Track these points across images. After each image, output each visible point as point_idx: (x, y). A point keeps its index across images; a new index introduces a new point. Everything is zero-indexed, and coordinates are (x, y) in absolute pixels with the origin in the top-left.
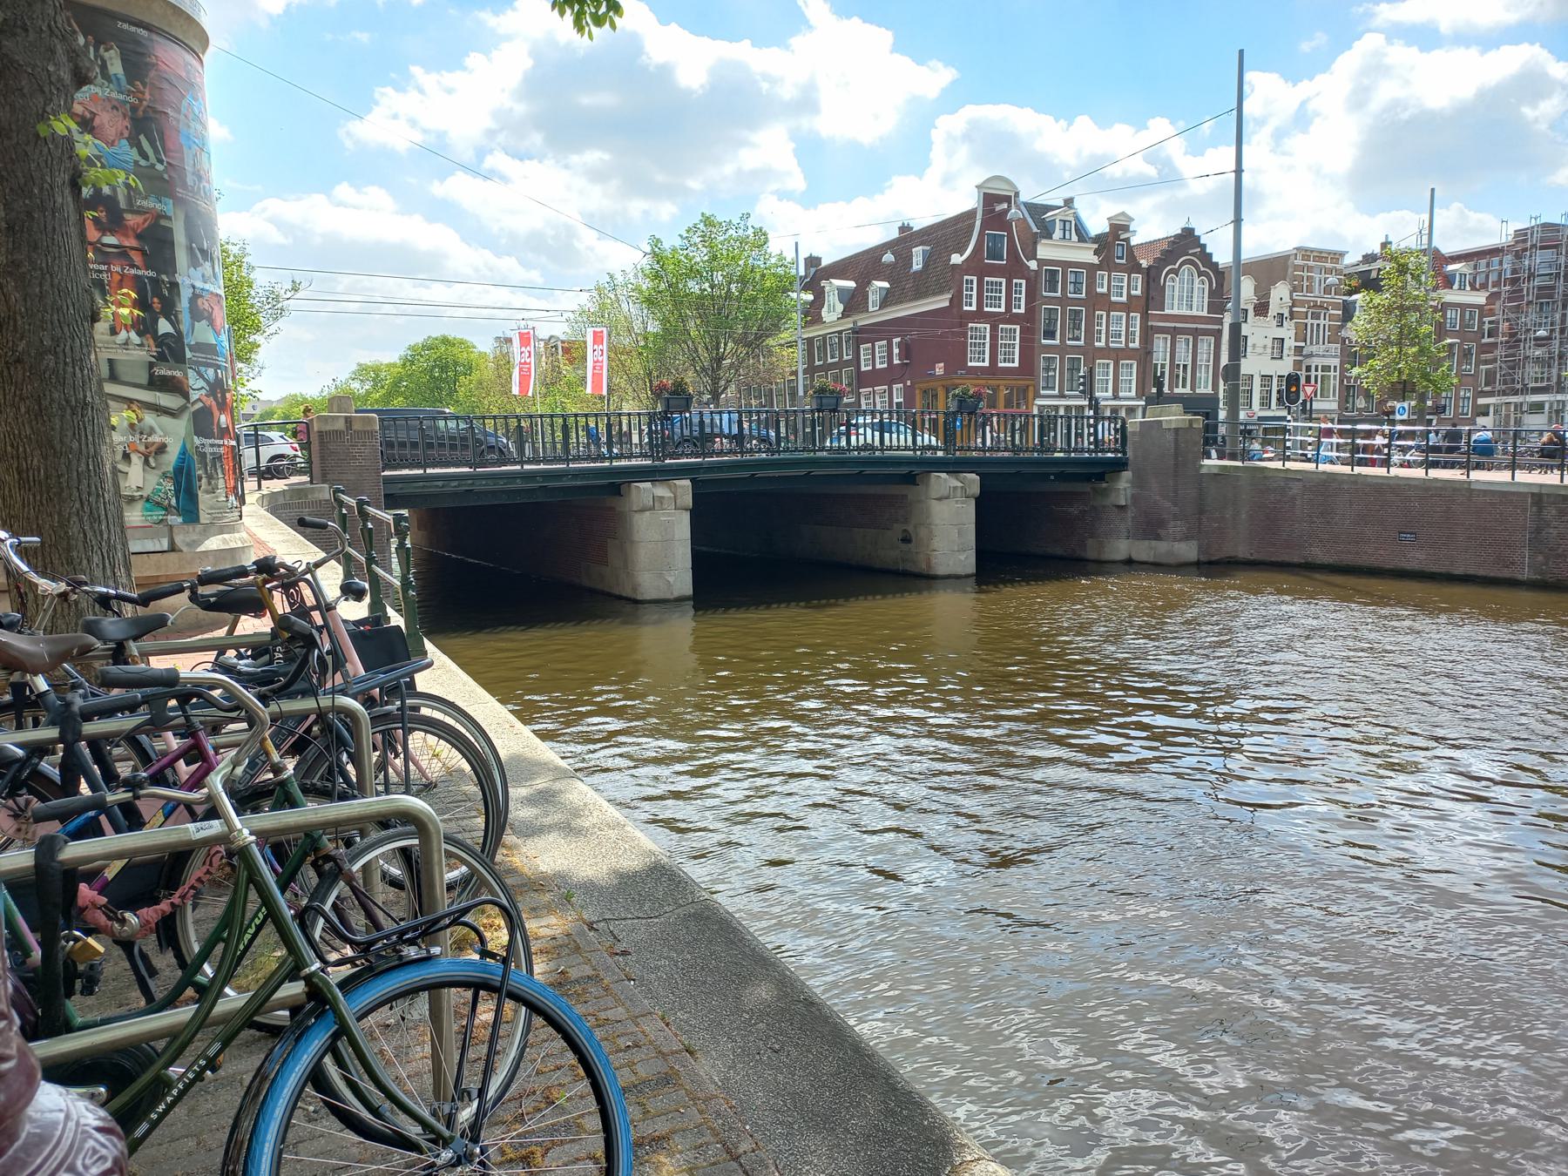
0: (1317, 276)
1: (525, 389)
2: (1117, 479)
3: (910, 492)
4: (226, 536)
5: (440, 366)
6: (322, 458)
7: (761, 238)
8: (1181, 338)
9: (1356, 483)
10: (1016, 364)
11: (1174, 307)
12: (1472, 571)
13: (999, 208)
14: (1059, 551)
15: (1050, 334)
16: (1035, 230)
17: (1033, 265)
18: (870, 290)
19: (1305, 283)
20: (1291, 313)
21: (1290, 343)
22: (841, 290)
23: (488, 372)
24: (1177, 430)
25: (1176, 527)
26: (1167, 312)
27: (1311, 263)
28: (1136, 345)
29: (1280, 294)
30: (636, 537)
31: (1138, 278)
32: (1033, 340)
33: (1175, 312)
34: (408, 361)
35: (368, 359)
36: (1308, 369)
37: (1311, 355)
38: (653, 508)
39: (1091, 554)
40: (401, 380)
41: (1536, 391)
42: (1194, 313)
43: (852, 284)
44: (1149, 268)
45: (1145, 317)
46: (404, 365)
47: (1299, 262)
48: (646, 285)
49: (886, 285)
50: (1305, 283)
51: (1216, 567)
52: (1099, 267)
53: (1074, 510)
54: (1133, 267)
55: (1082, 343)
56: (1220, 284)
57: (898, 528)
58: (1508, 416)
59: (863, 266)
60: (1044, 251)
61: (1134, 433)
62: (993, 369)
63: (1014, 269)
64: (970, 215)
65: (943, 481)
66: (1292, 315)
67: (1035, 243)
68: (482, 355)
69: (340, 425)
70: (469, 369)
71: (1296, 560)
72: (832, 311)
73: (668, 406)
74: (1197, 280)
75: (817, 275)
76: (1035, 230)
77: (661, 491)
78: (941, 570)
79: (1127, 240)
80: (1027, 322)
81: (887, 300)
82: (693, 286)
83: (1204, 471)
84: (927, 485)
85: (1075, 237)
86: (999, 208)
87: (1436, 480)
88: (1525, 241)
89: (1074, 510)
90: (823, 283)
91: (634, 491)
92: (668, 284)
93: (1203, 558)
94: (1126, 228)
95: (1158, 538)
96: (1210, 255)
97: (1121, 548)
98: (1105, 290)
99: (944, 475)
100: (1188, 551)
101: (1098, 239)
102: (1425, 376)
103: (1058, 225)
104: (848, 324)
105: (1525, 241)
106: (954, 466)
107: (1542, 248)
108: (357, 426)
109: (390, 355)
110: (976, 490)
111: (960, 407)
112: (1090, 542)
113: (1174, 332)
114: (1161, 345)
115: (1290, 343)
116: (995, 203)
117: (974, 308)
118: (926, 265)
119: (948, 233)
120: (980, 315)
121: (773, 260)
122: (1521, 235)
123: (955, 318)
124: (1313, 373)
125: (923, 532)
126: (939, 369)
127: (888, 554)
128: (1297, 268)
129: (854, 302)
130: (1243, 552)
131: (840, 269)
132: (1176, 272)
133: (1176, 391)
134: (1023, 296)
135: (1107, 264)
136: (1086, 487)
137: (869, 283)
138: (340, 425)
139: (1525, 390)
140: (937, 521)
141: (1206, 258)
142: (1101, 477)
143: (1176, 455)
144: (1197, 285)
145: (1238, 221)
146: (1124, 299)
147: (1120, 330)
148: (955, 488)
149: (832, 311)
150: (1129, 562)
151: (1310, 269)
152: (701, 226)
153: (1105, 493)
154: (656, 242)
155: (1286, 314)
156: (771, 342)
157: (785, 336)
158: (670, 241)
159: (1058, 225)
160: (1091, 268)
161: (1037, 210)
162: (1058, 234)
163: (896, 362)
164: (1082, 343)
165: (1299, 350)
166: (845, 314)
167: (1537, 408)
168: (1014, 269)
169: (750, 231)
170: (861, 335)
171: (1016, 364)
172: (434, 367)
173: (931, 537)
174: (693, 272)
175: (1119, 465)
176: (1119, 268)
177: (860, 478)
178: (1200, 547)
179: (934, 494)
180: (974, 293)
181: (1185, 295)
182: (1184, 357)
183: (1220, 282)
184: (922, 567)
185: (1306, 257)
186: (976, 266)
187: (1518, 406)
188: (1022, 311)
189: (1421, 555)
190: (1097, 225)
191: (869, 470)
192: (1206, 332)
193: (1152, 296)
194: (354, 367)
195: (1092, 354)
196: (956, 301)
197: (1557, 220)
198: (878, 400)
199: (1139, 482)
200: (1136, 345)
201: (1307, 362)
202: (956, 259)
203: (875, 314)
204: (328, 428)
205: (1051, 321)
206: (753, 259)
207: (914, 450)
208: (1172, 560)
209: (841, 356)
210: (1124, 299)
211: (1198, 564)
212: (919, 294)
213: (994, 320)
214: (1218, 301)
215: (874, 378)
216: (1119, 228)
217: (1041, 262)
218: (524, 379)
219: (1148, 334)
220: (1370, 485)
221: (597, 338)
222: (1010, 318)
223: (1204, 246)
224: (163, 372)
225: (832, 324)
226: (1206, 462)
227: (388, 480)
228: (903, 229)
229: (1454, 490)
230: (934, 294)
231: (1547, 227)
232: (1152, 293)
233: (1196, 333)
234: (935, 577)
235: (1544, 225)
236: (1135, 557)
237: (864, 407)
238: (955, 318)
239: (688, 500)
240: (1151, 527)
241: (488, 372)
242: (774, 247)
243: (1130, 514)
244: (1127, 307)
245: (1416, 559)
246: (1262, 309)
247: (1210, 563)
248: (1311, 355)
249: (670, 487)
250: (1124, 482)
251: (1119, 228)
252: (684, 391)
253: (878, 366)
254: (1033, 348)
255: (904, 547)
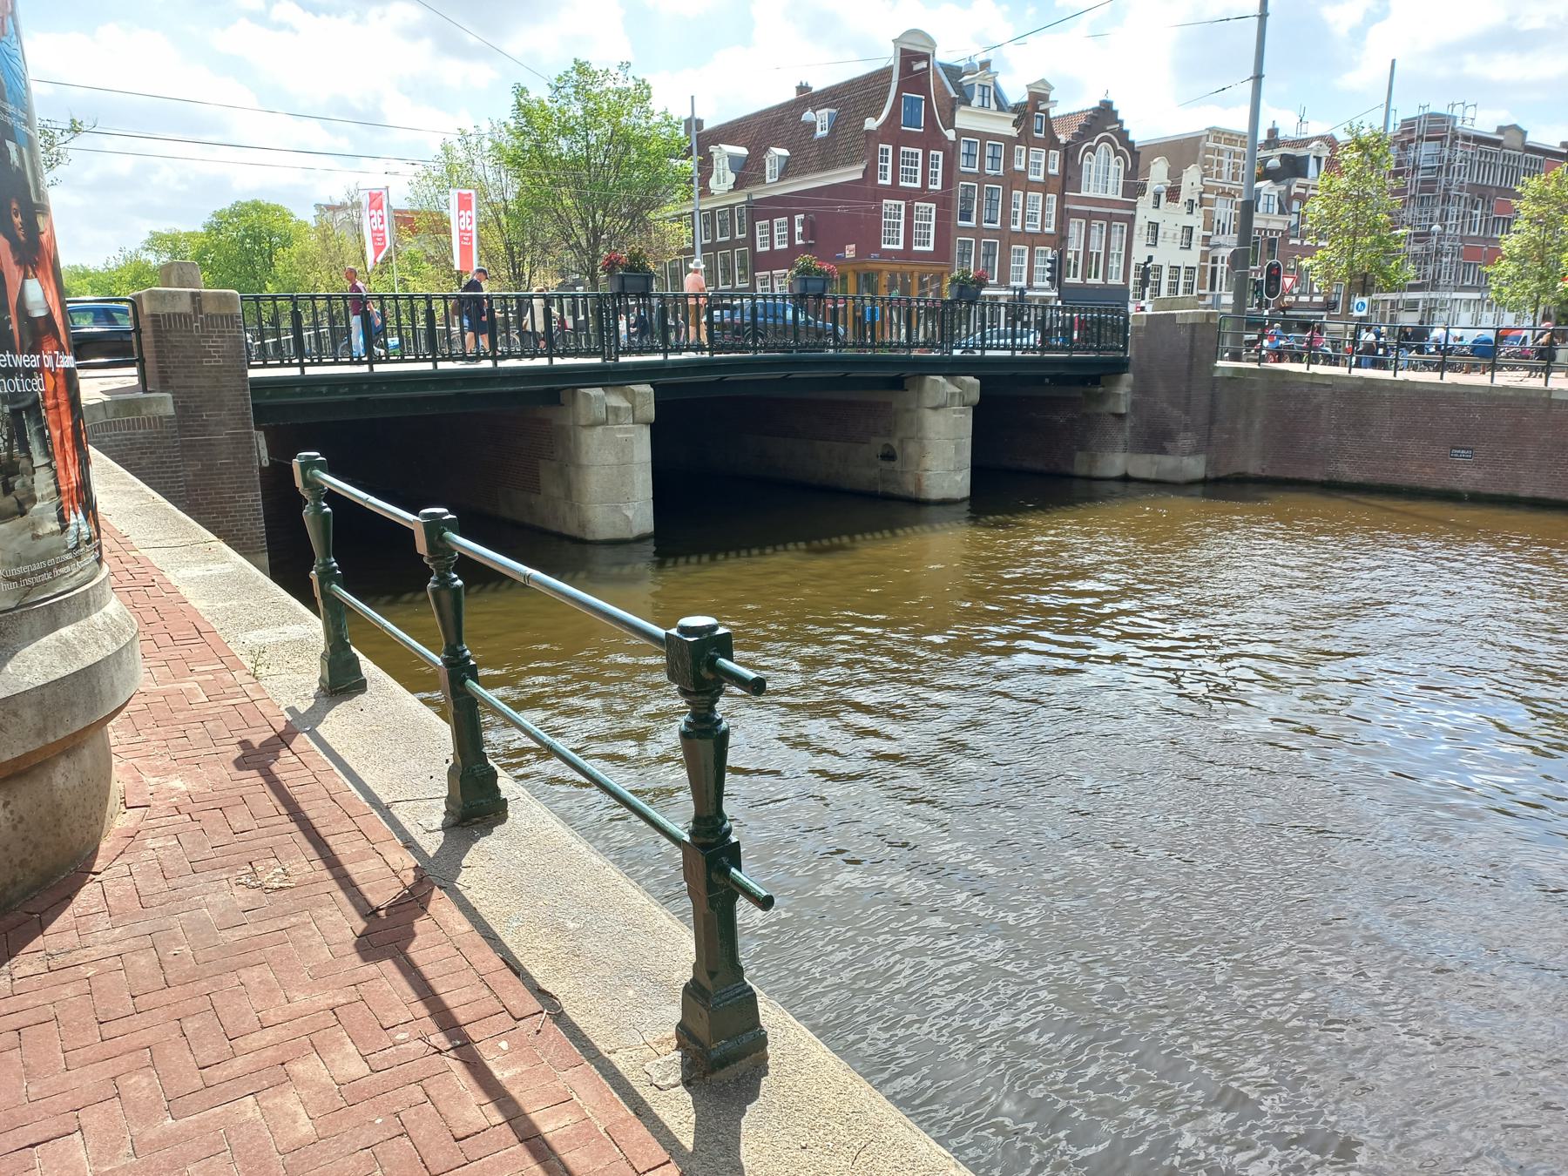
0: (1225, 159)
1: (372, 258)
2: (1116, 383)
3: (897, 399)
4: (66, 631)
5: (250, 240)
6: (160, 354)
7: (642, 93)
8: (1096, 223)
9: (1400, 390)
10: (931, 248)
11: (1091, 188)
12: (1542, 493)
13: (918, 66)
14: (1039, 465)
15: (966, 216)
16: (953, 95)
17: (951, 135)
18: (768, 158)
19: (1216, 169)
20: (1201, 199)
21: (1198, 232)
22: (732, 159)
23: (312, 243)
24: (1193, 325)
25: (1186, 440)
26: (1084, 194)
27: (1222, 146)
28: (1051, 229)
29: (1192, 178)
30: (584, 461)
31: (1056, 154)
32: (949, 218)
33: (1091, 194)
34: (214, 229)
35: (164, 227)
36: (1215, 260)
37: (1219, 246)
38: (605, 423)
39: (1081, 469)
40: (206, 251)
41: (1413, 288)
42: (1110, 195)
43: (743, 151)
44: (1068, 143)
45: (1062, 199)
46: (209, 234)
47: (1210, 144)
48: (509, 142)
49: (785, 152)
50: (1216, 169)
51: (1227, 486)
52: (1018, 141)
53: (1060, 419)
54: (1051, 142)
55: (998, 225)
56: (1136, 166)
57: (877, 444)
58: (1384, 313)
59: (757, 131)
60: (963, 119)
61: (1137, 329)
62: (908, 252)
63: (931, 139)
64: (885, 73)
65: (940, 386)
66: (1202, 202)
67: (953, 110)
68: (302, 225)
69: (185, 307)
70: (287, 242)
71: (1317, 477)
72: (722, 181)
73: (623, 286)
74: (1113, 160)
75: (704, 140)
76: (953, 95)
77: (615, 400)
78: (935, 493)
79: (1046, 112)
80: (943, 201)
81: (787, 171)
82: (563, 146)
83: (1217, 374)
84: (920, 389)
85: (994, 106)
86: (918, 66)
87: (1406, 381)
88: (1411, 131)
89: (1060, 419)
90: (712, 148)
91: (581, 402)
92: (533, 146)
93: (1211, 475)
94: (1045, 98)
95: (1163, 451)
96: (1127, 133)
97: (1116, 462)
98: (1022, 167)
99: (941, 379)
100: (1195, 467)
101: (1016, 109)
102: (1380, 269)
103: (977, 91)
104: (740, 198)
105: (1411, 131)
106: (952, 368)
107: (1428, 139)
108: (209, 308)
109: (192, 222)
110: (975, 396)
111: (960, 295)
112: (1079, 456)
113: (1089, 217)
114: (1075, 229)
115: (1198, 232)
116: (913, 63)
117: (888, 182)
118: (833, 129)
119: (853, 98)
120: (895, 192)
121: (656, 119)
122: (1408, 125)
123: (867, 192)
124: (1219, 265)
125: (911, 448)
126: (850, 251)
127: (863, 471)
128: (1208, 151)
129: (747, 172)
130: (1253, 467)
131: (728, 133)
132: (1093, 150)
133: (1089, 281)
134: (940, 170)
135: (1025, 138)
136: (1078, 392)
137: (766, 149)
138: (185, 307)
139: (1400, 289)
140: (932, 435)
141: (1123, 135)
142: (1096, 381)
143: (1191, 356)
144: (1113, 165)
145: (1258, 78)
146: (1041, 178)
147: (1035, 212)
148: (953, 395)
149: (722, 181)
150: (1126, 479)
151: (1220, 152)
152: (574, 75)
153: (1101, 399)
154: (521, 91)
155: (1197, 201)
156: (652, 215)
157: (670, 210)
158: (539, 92)
159: (977, 91)
160: (1010, 142)
161: (953, 72)
162: (976, 101)
163: (799, 242)
164: (998, 225)
165: (1206, 239)
166: (738, 185)
167: (1412, 306)
168: (931, 139)
169: (631, 84)
170: (760, 210)
171: (931, 248)
172: (244, 237)
173: (922, 453)
174: (565, 130)
175: (1120, 366)
176: (1037, 143)
177: (844, 383)
178: (1208, 463)
179: (928, 402)
180: (890, 165)
181: (1101, 176)
182: (1097, 246)
183: (1135, 159)
184: (910, 489)
185: (1217, 140)
186: (892, 132)
187: (1394, 304)
188: (939, 187)
189: (1477, 475)
190: (1016, 94)
191: (856, 373)
192: (1120, 218)
193: (1069, 178)
194: (147, 237)
195: (1008, 238)
196: (871, 173)
197: (1443, 111)
198: (776, 285)
199: (1143, 387)
200: (1051, 229)
201: (1213, 253)
202: (871, 124)
203: (773, 186)
204: (168, 310)
205: (967, 201)
206: (631, 120)
207: (1013, 350)
208: (1179, 478)
209: (733, 234)
210: (1041, 178)
211: (1204, 481)
212: (826, 164)
213: (909, 196)
214: (1134, 188)
215: (772, 260)
216: (1038, 98)
217: (961, 133)
218: (465, 250)
219: (1063, 217)
220: (1417, 392)
221: (464, 203)
222: (923, 194)
223: (1121, 122)
224: (264, 453)
225: (722, 197)
226: (1220, 363)
227: (258, 384)
228: (802, 89)
229: (1529, 399)
230: (844, 164)
231: (1436, 118)
232: (1069, 172)
233: (1110, 218)
234: (927, 503)
235: (1431, 115)
236: (1132, 473)
237: (777, 292)
238: (867, 192)
239: (650, 412)
240: (1155, 439)
241: (312, 243)
242: (656, 105)
243: (1128, 424)
244: (1044, 187)
245: (1469, 477)
246: (1173, 194)
247: (1217, 481)
248: (1219, 246)
249: (625, 395)
250: (1125, 386)
251: (1038, 98)
252: (643, 267)
253: (777, 247)
254: (948, 231)
255: (885, 465)
